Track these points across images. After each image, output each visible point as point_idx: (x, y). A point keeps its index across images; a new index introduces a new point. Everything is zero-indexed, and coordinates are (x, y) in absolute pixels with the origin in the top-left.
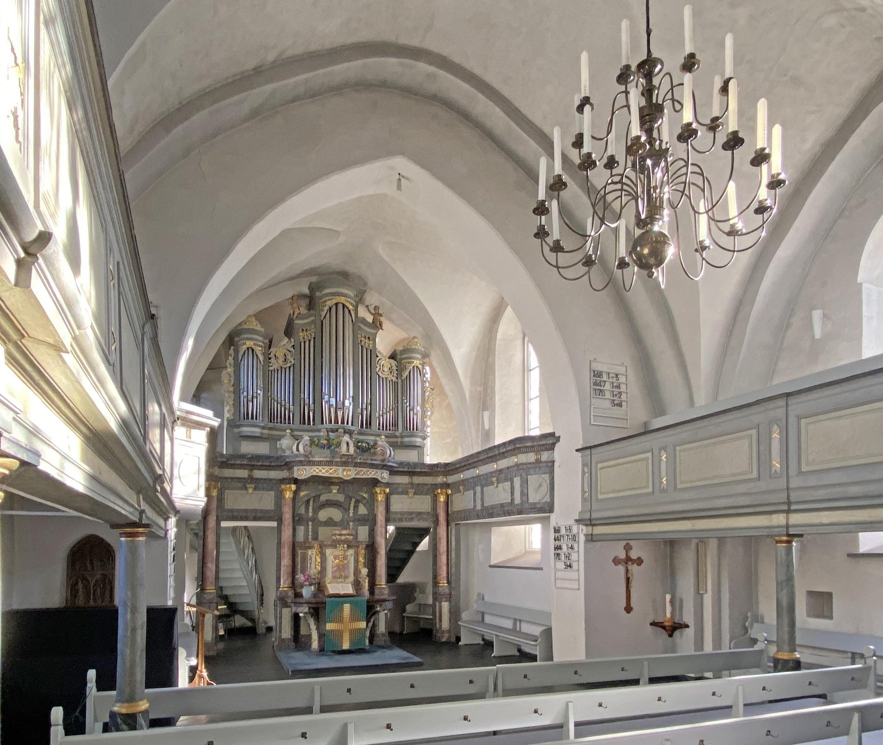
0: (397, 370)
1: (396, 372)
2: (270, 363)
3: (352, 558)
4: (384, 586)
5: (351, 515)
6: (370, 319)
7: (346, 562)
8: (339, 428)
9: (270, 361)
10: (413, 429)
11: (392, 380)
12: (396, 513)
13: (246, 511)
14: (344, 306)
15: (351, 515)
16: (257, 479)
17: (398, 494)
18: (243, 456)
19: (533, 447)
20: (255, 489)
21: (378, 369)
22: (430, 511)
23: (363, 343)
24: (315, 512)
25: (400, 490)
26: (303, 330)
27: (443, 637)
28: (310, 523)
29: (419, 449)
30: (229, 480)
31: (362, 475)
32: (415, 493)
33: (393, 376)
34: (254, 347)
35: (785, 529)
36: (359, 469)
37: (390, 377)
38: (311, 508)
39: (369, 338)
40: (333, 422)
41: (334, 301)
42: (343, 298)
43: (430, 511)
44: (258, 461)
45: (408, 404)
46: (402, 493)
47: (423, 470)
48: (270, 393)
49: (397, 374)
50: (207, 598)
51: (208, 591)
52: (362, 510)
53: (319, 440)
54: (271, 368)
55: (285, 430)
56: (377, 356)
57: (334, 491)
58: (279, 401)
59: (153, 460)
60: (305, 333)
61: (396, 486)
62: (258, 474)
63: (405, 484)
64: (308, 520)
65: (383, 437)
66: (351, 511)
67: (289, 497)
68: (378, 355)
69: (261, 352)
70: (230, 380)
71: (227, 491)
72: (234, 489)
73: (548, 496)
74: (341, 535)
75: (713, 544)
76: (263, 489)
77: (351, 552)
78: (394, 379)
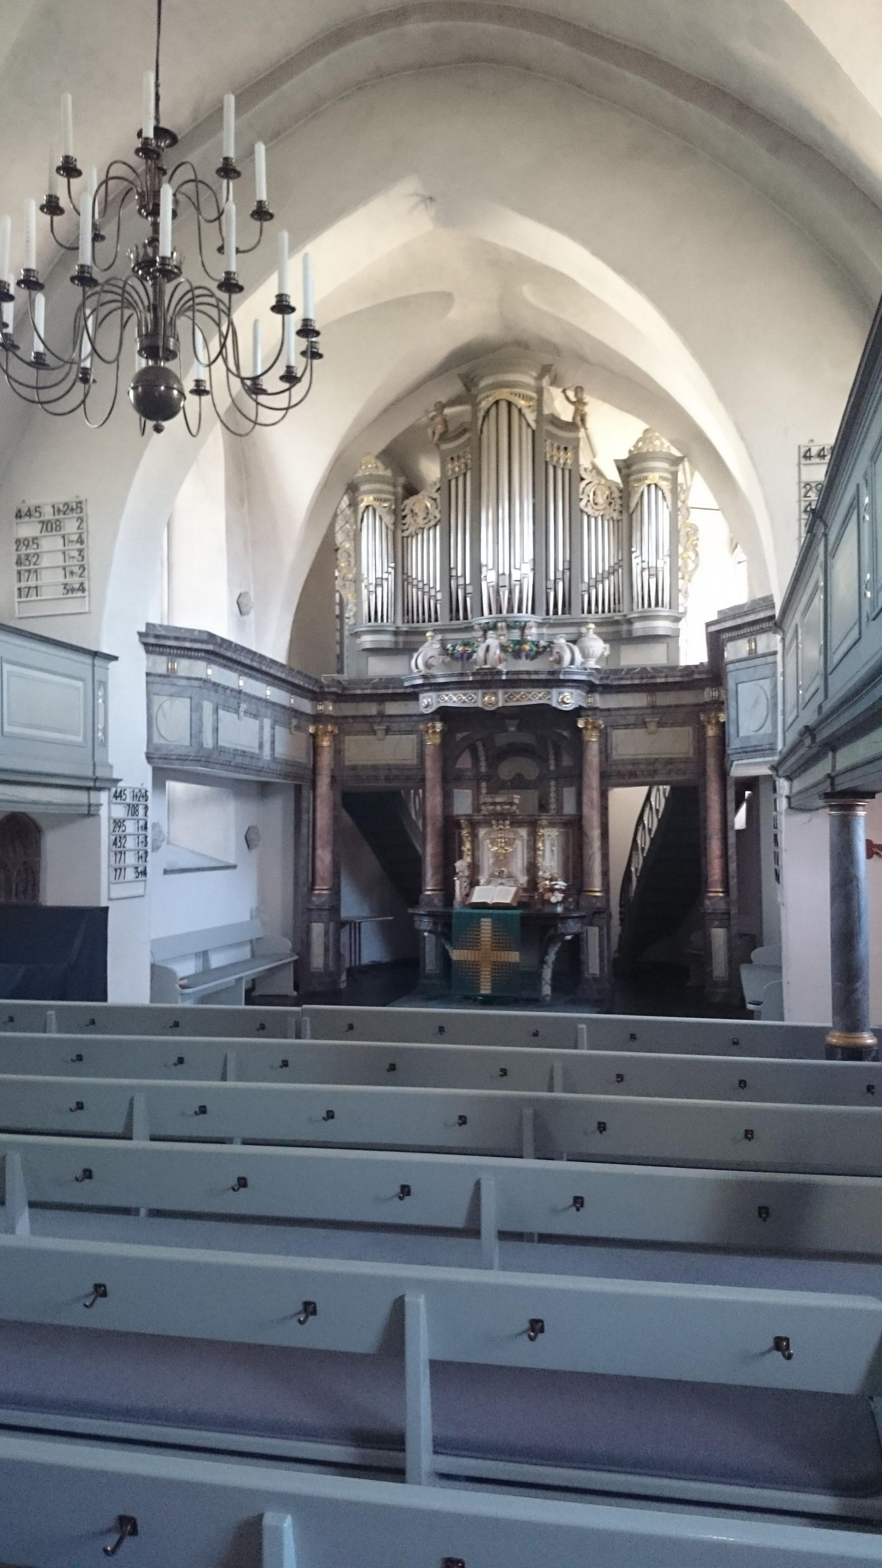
0: (621, 498)
1: (619, 502)
2: (404, 524)
4: (598, 894)
5: (552, 768)
6: (566, 413)
7: (510, 849)
8: (497, 622)
9: (404, 522)
10: (649, 605)
11: (612, 518)
14: (510, 404)
15: (552, 768)
16: (390, 716)
21: (582, 504)
23: (555, 459)
24: (490, 765)
26: (452, 459)
28: (484, 785)
29: (668, 640)
30: (350, 720)
31: (518, 700)
32: (660, 724)
35: (86, 808)
36: (511, 691)
38: (483, 758)
39: (566, 449)
41: (491, 400)
42: (506, 390)
47: (670, 680)
49: (621, 505)
50: (317, 903)
51: (711, 894)
52: (567, 761)
53: (454, 647)
54: (406, 534)
55: (424, 633)
56: (582, 479)
57: (512, 729)
58: (420, 585)
60: (562, 453)
65: (592, 626)
66: (552, 762)
68: (584, 475)
70: (349, 562)
71: (347, 738)
72: (358, 733)
73: (769, 723)
78: (616, 515)
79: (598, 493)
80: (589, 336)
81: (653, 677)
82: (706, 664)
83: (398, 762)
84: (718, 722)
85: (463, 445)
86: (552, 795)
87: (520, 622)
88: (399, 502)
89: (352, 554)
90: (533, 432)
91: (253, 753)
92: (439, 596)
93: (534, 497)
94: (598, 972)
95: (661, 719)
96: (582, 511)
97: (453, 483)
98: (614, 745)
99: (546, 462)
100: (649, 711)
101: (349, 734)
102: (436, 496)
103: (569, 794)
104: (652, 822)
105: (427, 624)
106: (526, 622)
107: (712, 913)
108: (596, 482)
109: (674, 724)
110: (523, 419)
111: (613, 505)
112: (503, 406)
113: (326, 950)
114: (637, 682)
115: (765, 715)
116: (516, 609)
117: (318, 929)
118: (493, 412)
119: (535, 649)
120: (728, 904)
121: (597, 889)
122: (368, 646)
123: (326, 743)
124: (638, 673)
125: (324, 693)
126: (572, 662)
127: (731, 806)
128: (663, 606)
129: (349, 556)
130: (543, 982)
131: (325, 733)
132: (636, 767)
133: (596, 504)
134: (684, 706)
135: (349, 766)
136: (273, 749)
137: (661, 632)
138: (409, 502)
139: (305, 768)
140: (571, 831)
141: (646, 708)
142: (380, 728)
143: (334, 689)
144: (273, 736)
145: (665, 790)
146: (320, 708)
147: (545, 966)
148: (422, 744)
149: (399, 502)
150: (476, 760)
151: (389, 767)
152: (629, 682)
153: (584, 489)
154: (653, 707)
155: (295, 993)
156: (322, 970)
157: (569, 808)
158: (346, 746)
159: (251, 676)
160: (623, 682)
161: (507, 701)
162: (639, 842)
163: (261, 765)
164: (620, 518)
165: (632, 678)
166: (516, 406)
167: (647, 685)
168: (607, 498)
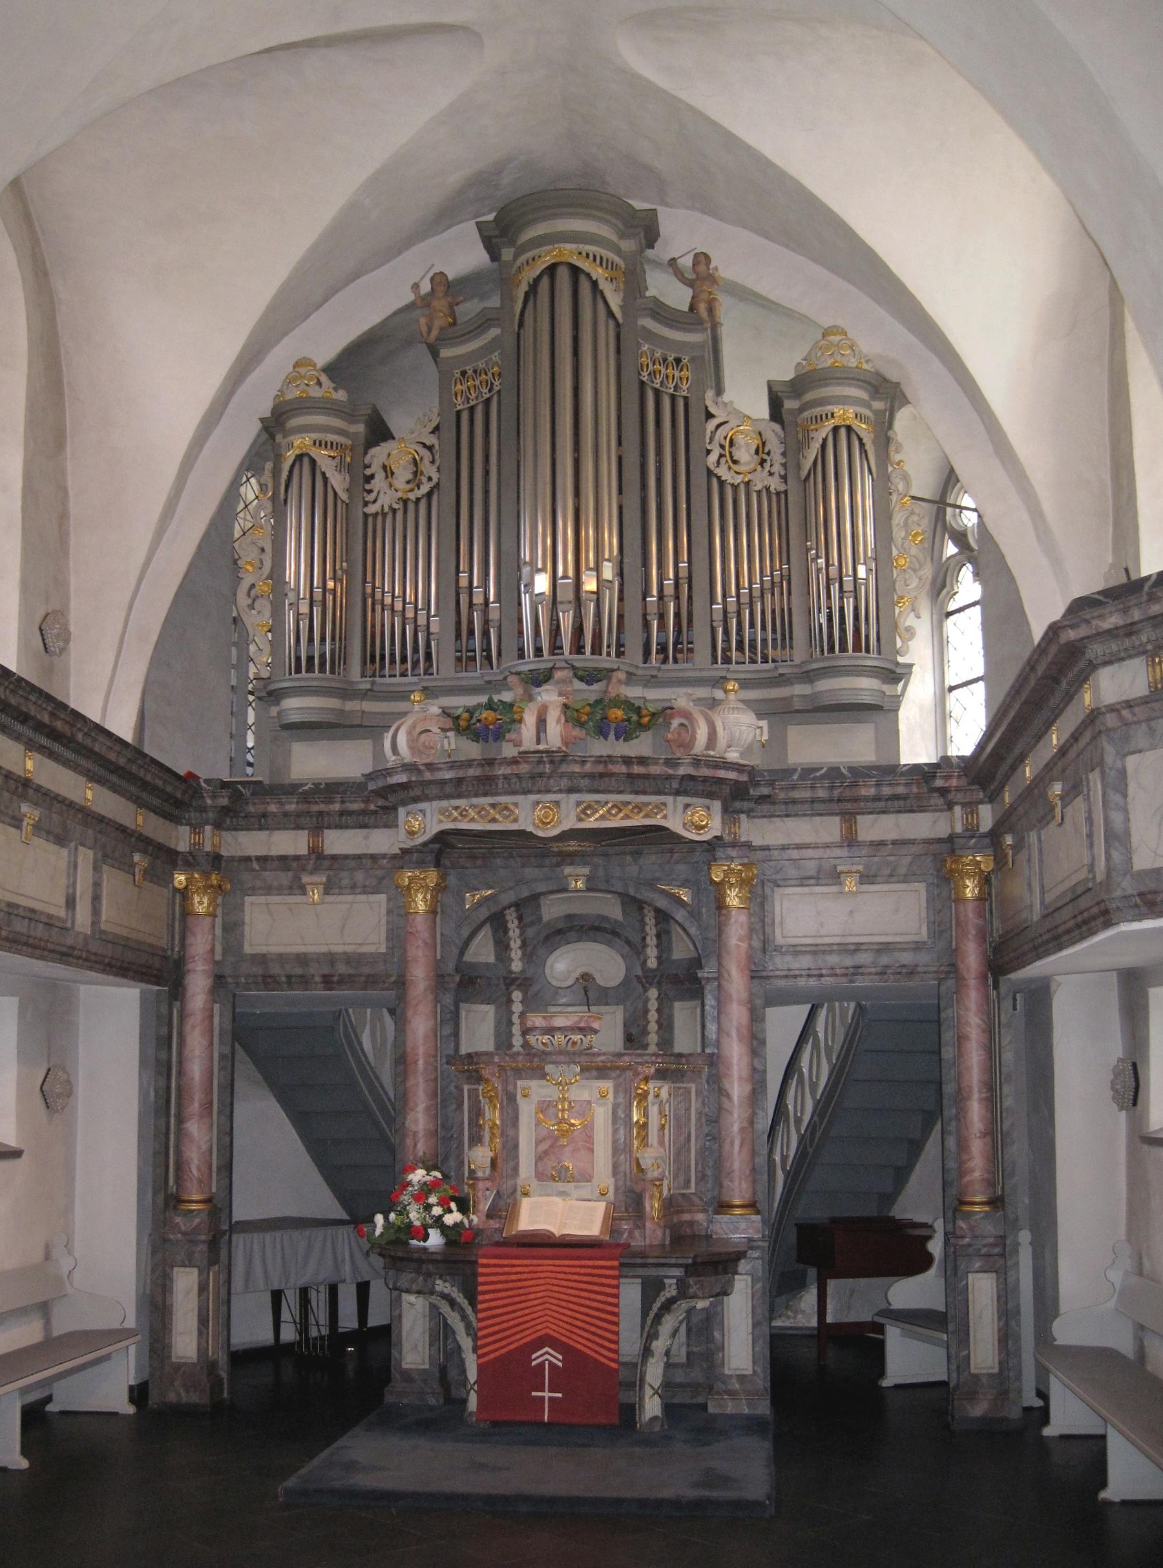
2: (370, 492)
9: (368, 487)
11: (768, 489)
12: (796, 951)
14: (575, 271)
15: (652, 963)
16: (334, 858)
18: (292, 789)
19: (1130, 630)
20: (328, 890)
21: (713, 458)
24: (530, 954)
26: (464, 373)
28: (517, 996)
30: (256, 866)
32: (866, 878)
33: (771, 474)
34: (314, 452)
37: (760, 480)
38: (515, 944)
40: (545, 651)
44: (331, 801)
45: (821, 561)
46: (817, 879)
48: (369, 586)
49: (784, 465)
54: (371, 509)
56: (710, 416)
59: (780, 1138)
62: (339, 842)
64: (511, 981)
66: (652, 952)
68: (712, 410)
69: (334, 463)
70: (261, 561)
71: (248, 900)
72: (268, 890)
75: (511, 917)
76: (353, 889)
79: (740, 440)
80: (732, 142)
83: (349, 949)
85: (487, 349)
86: (653, 1016)
91: (50, 916)
92: (434, 628)
93: (620, 443)
96: (710, 473)
97: (465, 416)
98: (777, 920)
101: (253, 891)
102: (431, 440)
105: (410, 679)
109: (891, 877)
111: (767, 466)
113: (203, 1321)
116: (588, 649)
118: (545, 282)
122: (294, 718)
124: (822, 777)
128: (868, 651)
133: (735, 462)
134: (912, 842)
136: (96, 912)
137: (866, 699)
138: (378, 455)
139: (165, 958)
144: (97, 885)
149: (360, 449)
150: (502, 946)
151: (331, 958)
153: (713, 433)
156: (195, 1360)
159: (51, 755)
161: (580, 820)
163: (69, 941)
164: (782, 488)
168: (757, 452)
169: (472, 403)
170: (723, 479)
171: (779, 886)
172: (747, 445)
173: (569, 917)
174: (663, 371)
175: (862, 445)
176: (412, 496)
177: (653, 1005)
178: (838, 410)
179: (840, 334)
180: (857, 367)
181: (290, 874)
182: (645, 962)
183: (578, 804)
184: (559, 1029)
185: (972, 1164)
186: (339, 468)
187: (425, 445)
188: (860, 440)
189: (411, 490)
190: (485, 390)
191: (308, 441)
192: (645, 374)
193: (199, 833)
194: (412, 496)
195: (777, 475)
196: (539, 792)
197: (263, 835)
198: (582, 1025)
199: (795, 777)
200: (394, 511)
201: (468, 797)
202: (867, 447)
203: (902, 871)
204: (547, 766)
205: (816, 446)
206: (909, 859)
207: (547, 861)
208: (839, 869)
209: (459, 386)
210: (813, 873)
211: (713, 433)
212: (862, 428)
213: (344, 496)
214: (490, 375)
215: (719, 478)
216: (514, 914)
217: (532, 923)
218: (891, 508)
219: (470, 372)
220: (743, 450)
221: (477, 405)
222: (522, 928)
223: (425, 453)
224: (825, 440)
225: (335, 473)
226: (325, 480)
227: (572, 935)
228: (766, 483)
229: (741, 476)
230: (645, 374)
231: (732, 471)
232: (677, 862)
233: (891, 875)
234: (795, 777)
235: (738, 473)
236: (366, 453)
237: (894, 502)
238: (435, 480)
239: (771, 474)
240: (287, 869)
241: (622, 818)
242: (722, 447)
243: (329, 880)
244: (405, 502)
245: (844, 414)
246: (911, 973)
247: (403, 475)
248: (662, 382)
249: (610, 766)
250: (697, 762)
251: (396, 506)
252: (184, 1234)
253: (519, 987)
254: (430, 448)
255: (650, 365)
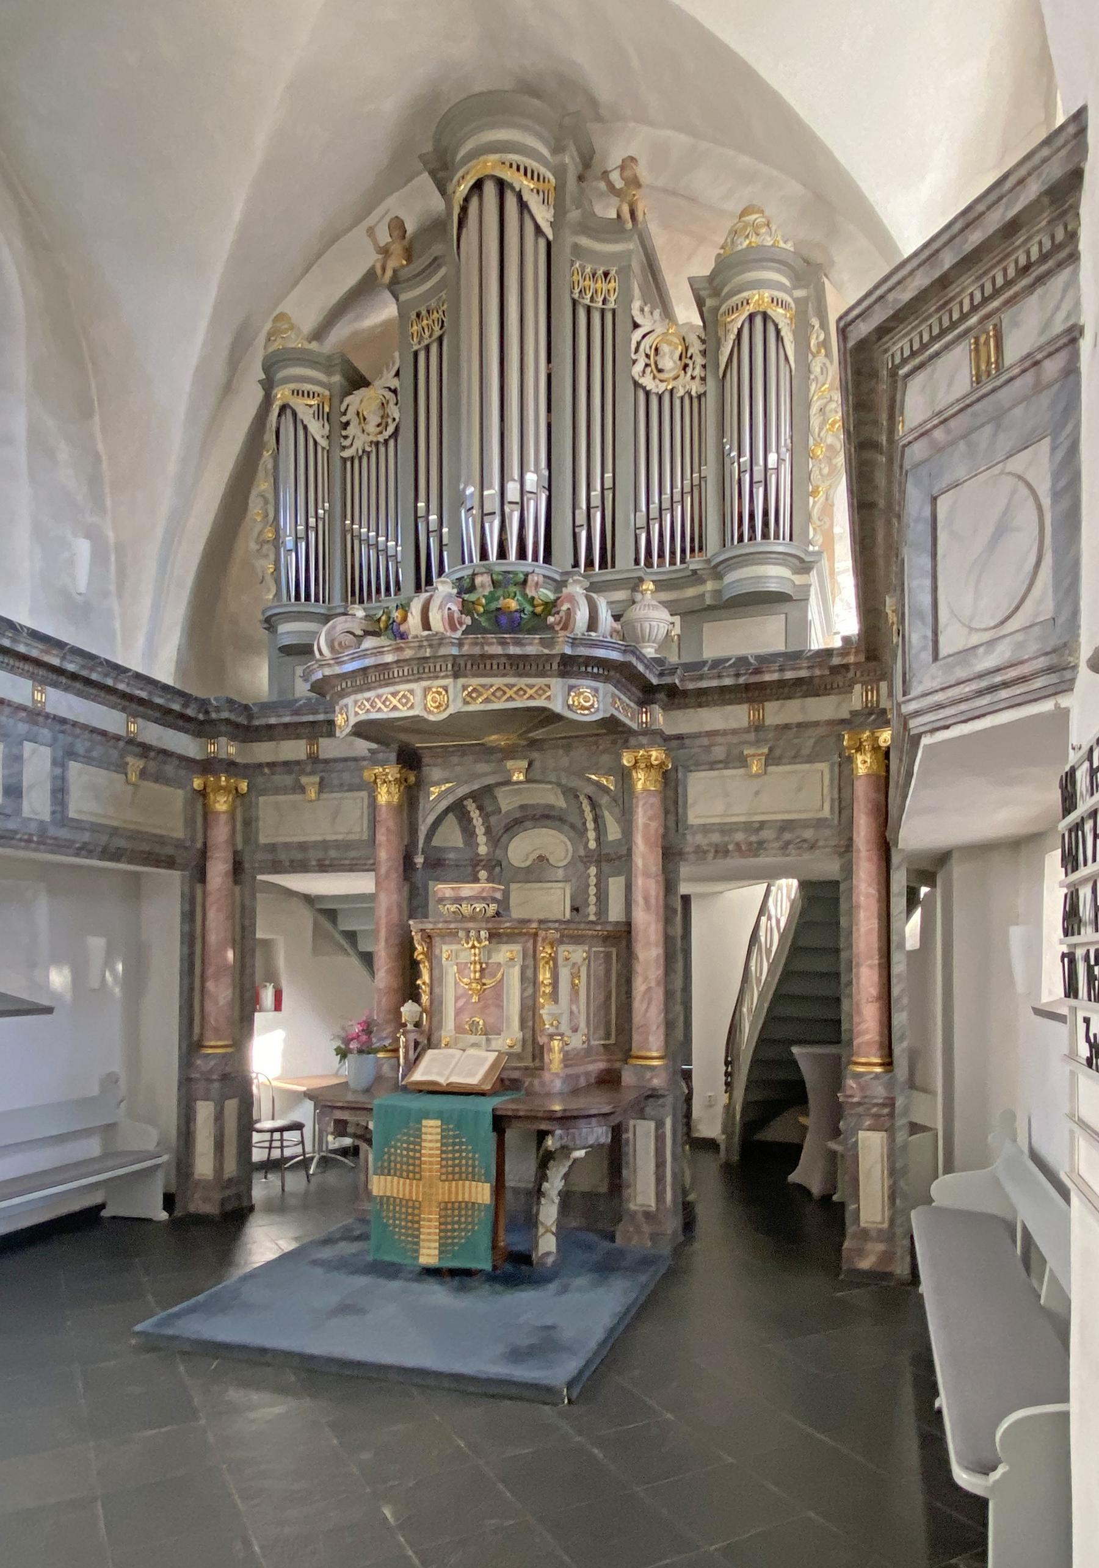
1: (699, 360)
2: (346, 437)
3: (516, 971)
4: (655, 1063)
9: (344, 433)
11: (689, 393)
12: (706, 829)
13: (303, 846)
15: (592, 845)
16: (326, 761)
17: (712, 766)
22: (826, 813)
24: (495, 841)
25: (719, 752)
26: (418, 315)
27: (860, 1252)
29: (787, 607)
30: (266, 770)
32: (771, 760)
38: (480, 830)
41: (470, 181)
42: (494, 157)
43: (826, 813)
47: (789, 675)
49: (704, 366)
50: (203, 1069)
54: (346, 454)
56: (636, 326)
61: (705, 741)
63: (734, 732)
67: (389, 803)
68: (639, 320)
71: (261, 799)
72: (277, 791)
74: (458, 900)
75: (470, 805)
77: (506, 953)
79: (665, 348)
81: (757, 671)
82: (855, 639)
84: (876, 748)
87: (515, 574)
88: (336, 401)
89: (272, 500)
90: (549, 245)
93: (549, 360)
94: (653, 1203)
95: (771, 750)
96: (636, 385)
99: (574, 302)
100: (752, 736)
103: (615, 886)
104: (772, 938)
106: (526, 575)
107: (859, 1104)
108: (660, 330)
109: (795, 759)
110: (525, 212)
112: (490, 189)
114: (728, 681)
115: (1032, 559)
117: (204, 1111)
119: (528, 608)
120: (890, 1086)
121: (655, 1054)
123: (221, 804)
125: (212, 722)
126: (592, 625)
127: (899, 903)
129: (266, 502)
130: (541, 1230)
131: (219, 789)
132: (726, 839)
133: (660, 371)
134: (816, 724)
135: (265, 845)
137: (773, 587)
138: (354, 400)
140: (614, 950)
141: (747, 731)
142: (310, 781)
143: (225, 715)
145: (789, 888)
146: (211, 748)
147: (543, 1201)
148: (373, 804)
149: (336, 401)
150: (469, 832)
152: (714, 683)
153: (639, 344)
154: (758, 727)
155: (164, 1216)
157: (615, 913)
158: (261, 814)
160: (704, 684)
161: (466, 703)
162: (753, 968)
165: (720, 677)
166: (513, 189)
167: (747, 687)
168: (680, 358)
169: (426, 342)
170: (648, 388)
171: (691, 771)
172: (672, 353)
173: (522, 807)
174: (592, 286)
175: (778, 332)
176: (381, 439)
177: (593, 880)
178: (755, 296)
179: (757, 213)
180: (773, 246)
181: (294, 776)
182: (587, 843)
183: (465, 688)
184: (466, 898)
185: (863, 1026)
186: (319, 414)
187: (390, 389)
188: (776, 326)
189: (381, 433)
190: (437, 328)
191: (287, 392)
192: (577, 291)
193: (214, 744)
194: (381, 439)
195: (698, 379)
196: (429, 678)
197: (272, 744)
198: (484, 894)
199: (706, 669)
200: (369, 454)
201: (375, 688)
202: (783, 333)
203: (806, 751)
204: (428, 650)
205: (732, 337)
206: (812, 741)
207: (493, 757)
208: (745, 752)
209: (415, 328)
210: (721, 758)
211: (639, 344)
212: (778, 314)
213: (323, 443)
214: (441, 313)
215: (644, 388)
216: (474, 805)
217: (493, 813)
218: (811, 396)
219: (424, 313)
220: (667, 357)
221: (432, 342)
222: (486, 816)
223: (390, 395)
224: (740, 332)
225: (312, 420)
226: (305, 428)
227: (529, 824)
228: (687, 387)
229: (665, 384)
230: (577, 291)
231: (657, 381)
232: (603, 752)
233: (795, 757)
234: (706, 669)
235: (661, 381)
236: (341, 402)
237: (812, 392)
238: (397, 420)
239: (693, 378)
240: (290, 772)
241: (528, 698)
242: (648, 356)
243: (322, 779)
244: (377, 444)
245: (759, 299)
246: (812, 848)
247: (374, 420)
248: (592, 297)
249: (486, 648)
250: (574, 642)
251: (368, 449)
252: (202, 1073)
253: (484, 868)
254: (395, 391)
255: (581, 282)
